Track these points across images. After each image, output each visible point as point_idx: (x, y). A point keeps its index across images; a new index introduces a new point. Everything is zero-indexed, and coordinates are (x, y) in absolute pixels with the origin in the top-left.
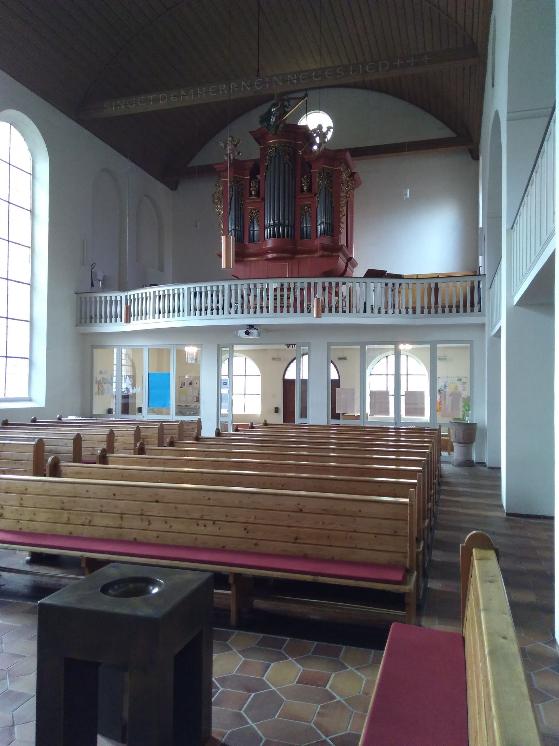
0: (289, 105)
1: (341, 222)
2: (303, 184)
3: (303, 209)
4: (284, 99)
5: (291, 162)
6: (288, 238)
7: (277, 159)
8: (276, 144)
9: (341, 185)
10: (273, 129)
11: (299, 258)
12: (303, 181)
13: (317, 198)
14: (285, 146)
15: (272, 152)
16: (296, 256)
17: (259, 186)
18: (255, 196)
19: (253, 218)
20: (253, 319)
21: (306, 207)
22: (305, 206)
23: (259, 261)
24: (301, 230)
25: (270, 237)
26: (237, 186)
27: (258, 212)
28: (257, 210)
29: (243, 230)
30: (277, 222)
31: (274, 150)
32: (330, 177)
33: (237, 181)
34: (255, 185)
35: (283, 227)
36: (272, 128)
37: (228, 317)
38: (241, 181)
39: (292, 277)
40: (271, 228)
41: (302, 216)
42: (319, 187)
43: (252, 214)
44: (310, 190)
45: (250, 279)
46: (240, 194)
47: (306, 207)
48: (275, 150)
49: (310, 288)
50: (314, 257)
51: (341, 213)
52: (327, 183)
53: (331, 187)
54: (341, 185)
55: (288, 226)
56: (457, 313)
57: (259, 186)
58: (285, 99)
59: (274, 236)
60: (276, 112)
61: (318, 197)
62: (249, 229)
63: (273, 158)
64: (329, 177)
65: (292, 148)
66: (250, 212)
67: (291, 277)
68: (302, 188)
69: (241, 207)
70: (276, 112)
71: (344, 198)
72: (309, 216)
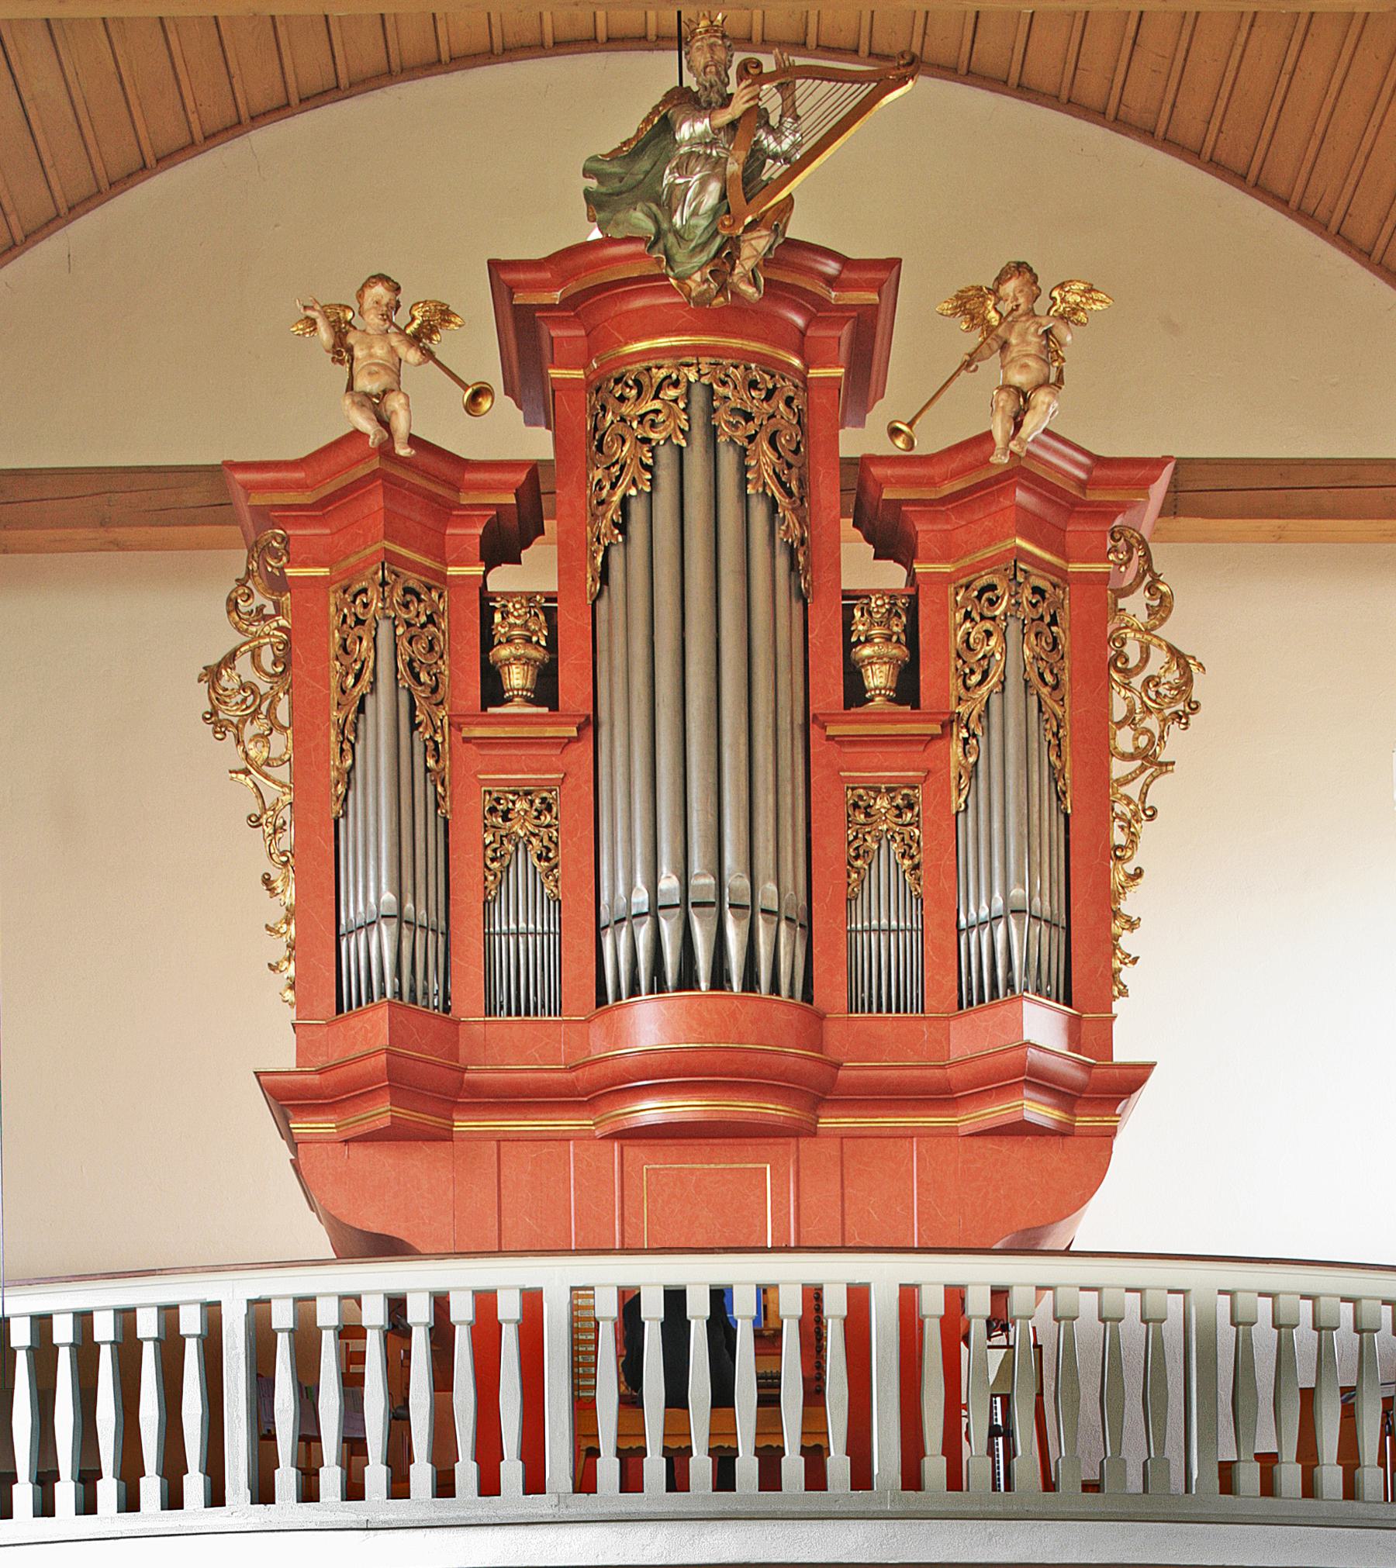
0: (790, 110)
1: (1116, 914)
2: (867, 651)
3: (868, 815)
4: (759, 65)
5: (789, 493)
6: (778, 994)
7: (696, 461)
8: (688, 365)
9: (1115, 676)
10: (703, 257)
11: (845, 1136)
12: (861, 628)
13: (956, 749)
14: (753, 385)
15: (661, 417)
16: (463, 1125)
17: (552, 645)
18: (529, 701)
19: (511, 848)
20: (665, 1530)
21: (882, 804)
22: (878, 791)
23: (564, 1139)
24: (851, 946)
25: (658, 984)
26: (409, 625)
27: (549, 809)
28: (544, 800)
29: (442, 923)
30: (708, 886)
31: (675, 401)
32: (1047, 619)
33: (407, 590)
34: (525, 626)
35: (746, 923)
36: (694, 252)
37: (572, 1512)
38: (429, 589)
39: (799, 1249)
40: (665, 926)
41: (857, 858)
42: (975, 679)
43: (506, 819)
44: (907, 689)
45: (500, 1253)
46: (424, 677)
47: (885, 804)
48: (682, 405)
49: (406, 1333)
50: (951, 1133)
51: (1119, 858)
52: (1037, 658)
53: (1055, 688)
54: (1115, 676)
55: (748, 910)
56: (1263, 1498)
57: (552, 645)
58: (765, 70)
59: (687, 979)
60: (700, 150)
61: (966, 741)
62: (487, 921)
63: (666, 455)
64: (1041, 618)
65: (789, 401)
66: (492, 810)
67: (792, 1245)
68: (853, 675)
69: (427, 770)
70: (700, 150)
71: (1138, 763)
72: (907, 862)
